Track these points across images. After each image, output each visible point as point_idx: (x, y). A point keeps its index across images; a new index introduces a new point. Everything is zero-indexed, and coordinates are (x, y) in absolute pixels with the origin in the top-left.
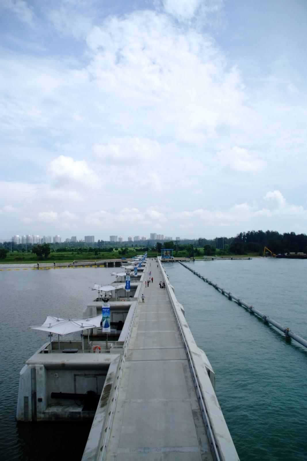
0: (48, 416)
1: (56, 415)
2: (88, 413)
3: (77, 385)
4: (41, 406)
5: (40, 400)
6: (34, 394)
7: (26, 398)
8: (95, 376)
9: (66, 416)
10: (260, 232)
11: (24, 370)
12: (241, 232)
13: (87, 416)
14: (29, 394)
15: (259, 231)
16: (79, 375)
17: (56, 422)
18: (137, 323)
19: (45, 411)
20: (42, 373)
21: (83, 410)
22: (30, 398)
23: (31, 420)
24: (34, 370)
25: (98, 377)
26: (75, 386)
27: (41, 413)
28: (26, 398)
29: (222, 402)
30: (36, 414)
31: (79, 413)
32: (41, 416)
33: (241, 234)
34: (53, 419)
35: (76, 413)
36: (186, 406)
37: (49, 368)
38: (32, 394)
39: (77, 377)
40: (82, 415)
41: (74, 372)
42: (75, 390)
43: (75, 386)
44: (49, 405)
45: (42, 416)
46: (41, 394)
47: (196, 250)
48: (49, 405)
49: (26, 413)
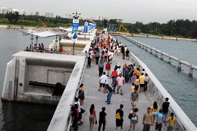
0: (26, 97)
1: (32, 97)
2: (56, 98)
3: (49, 78)
4: (21, 89)
5: (21, 85)
6: (16, 80)
7: (11, 82)
8: (63, 72)
9: (40, 99)
10: (187, 21)
11: (11, 63)
12: (128, 114)
13: (55, 100)
14: (13, 80)
15: (187, 20)
16: (51, 70)
17: (32, 104)
18: (23, 61)
19: (26, 94)
20: (23, 64)
21: (53, 95)
22: (13, 82)
23: (13, 99)
24: (17, 62)
25: (65, 73)
26: (47, 78)
27: (20, 94)
28: (11, 82)
29: (161, 81)
30: (17, 95)
31: (49, 97)
32: (20, 97)
33: (171, 21)
34: (30, 100)
35: (47, 97)
36: (192, 42)
37: (30, 63)
38: (15, 80)
39: (50, 72)
40: (51, 99)
41: (48, 68)
42: (47, 82)
43: (47, 78)
44: (26, 90)
45: (22, 96)
46: (21, 80)
47: (84, 25)
48: (26, 90)
49: (9, 94)
